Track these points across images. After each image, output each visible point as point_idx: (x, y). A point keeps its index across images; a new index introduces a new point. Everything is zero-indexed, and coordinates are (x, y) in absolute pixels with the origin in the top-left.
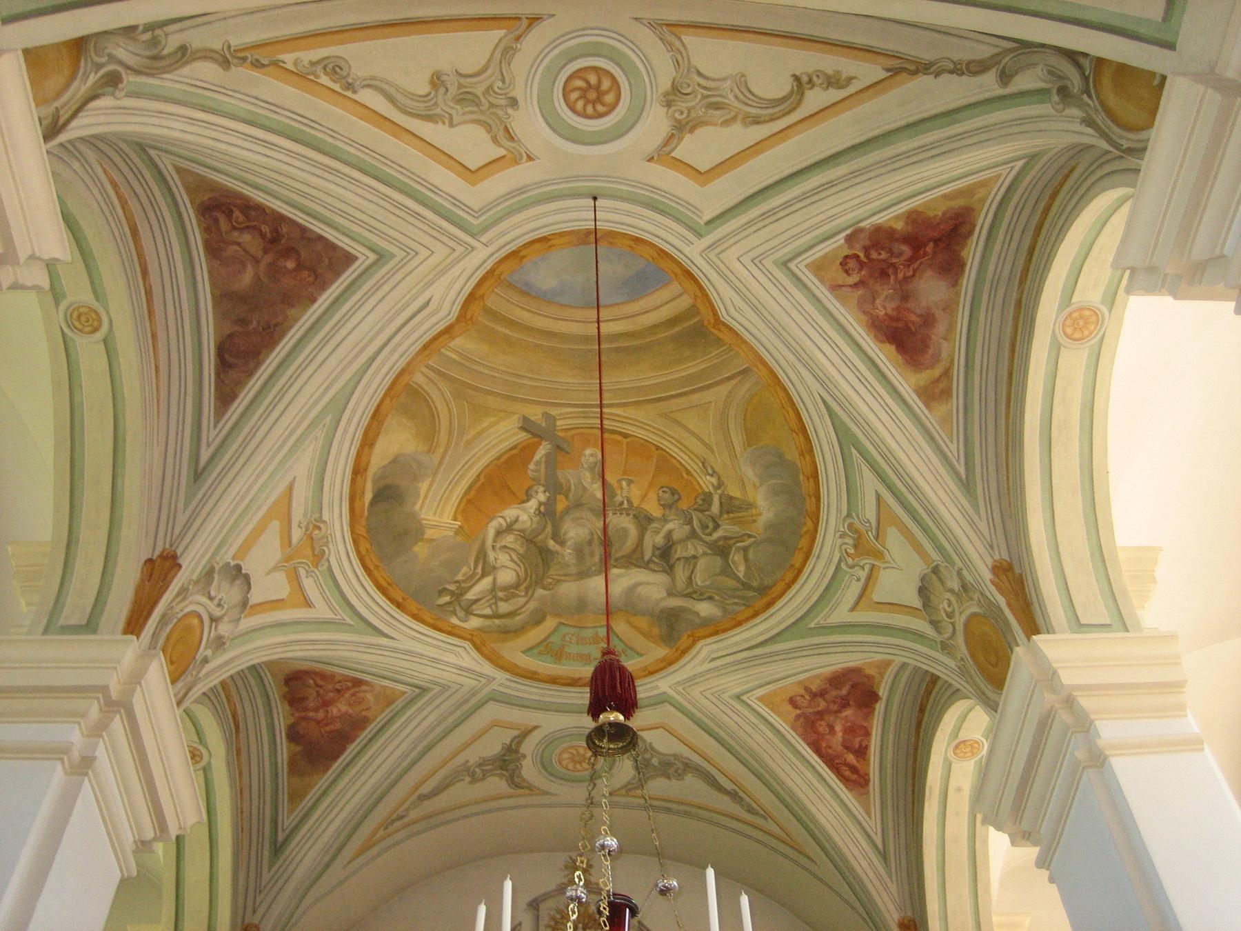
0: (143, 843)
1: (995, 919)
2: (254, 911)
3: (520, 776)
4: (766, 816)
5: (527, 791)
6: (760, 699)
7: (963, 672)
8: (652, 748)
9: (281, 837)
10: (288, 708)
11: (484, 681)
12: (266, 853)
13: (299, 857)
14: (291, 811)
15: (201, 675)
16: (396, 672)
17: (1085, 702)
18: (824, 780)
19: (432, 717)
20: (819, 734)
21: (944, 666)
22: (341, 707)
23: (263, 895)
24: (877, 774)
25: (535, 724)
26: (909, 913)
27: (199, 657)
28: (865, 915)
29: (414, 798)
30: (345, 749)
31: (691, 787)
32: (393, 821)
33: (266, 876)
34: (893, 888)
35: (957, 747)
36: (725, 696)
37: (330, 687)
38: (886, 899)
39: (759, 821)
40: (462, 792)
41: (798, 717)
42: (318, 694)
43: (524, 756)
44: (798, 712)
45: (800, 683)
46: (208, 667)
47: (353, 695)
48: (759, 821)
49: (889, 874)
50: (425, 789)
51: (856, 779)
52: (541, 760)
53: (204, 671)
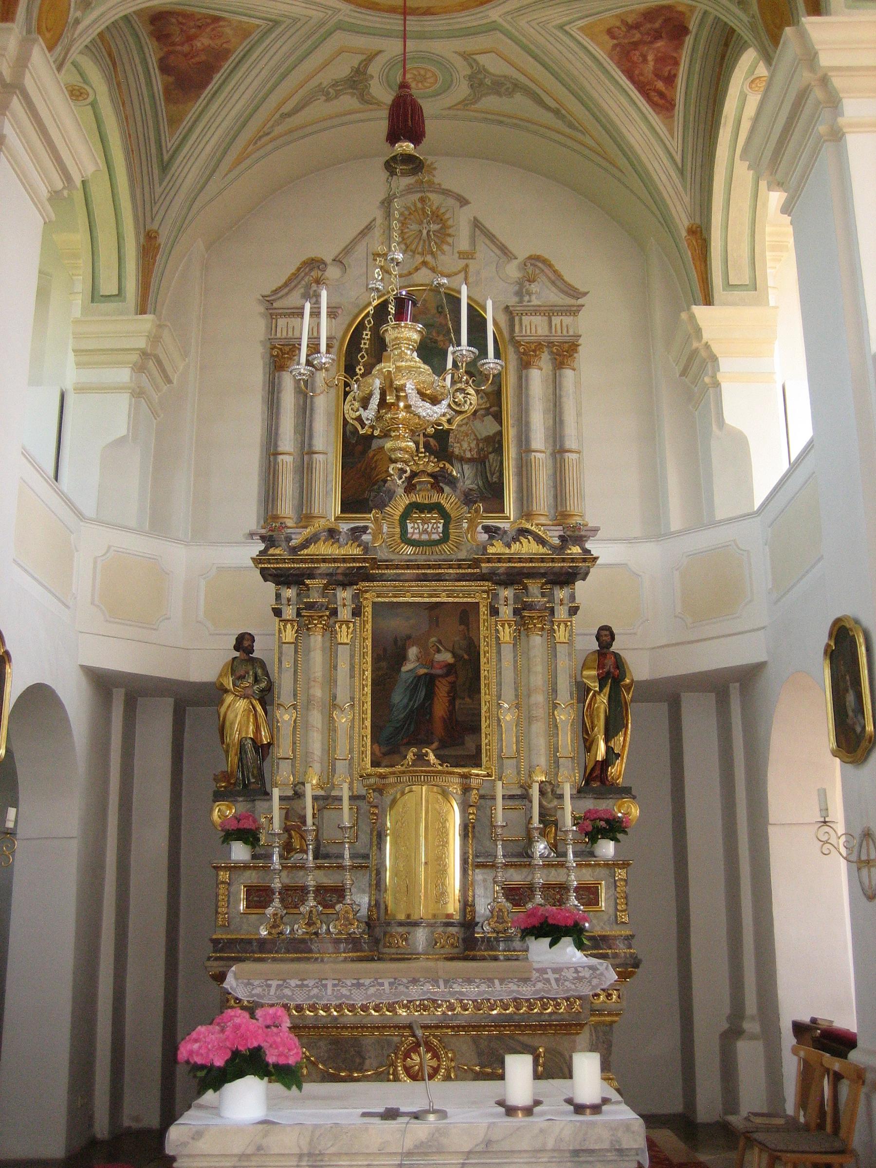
0: (55, 192)
1: (768, 229)
2: (153, 220)
3: (369, 93)
4: (584, 132)
5: (375, 107)
6: (581, 29)
7: (753, 28)
8: (485, 70)
9: (166, 158)
10: (156, 43)
11: (330, 12)
12: (156, 171)
13: (183, 175)
14: (172, 134)
15: (75, 36)
16: (249, 9)
17: (837, 82)
18: (635, 103)
19: (284, 49)
20: (633, 62)
21: (738, 20)
22: (203, 41)
23: (158, 204)
24: (682, 100)
25: (378, 49)
26: (698, 221)
27: (71, 20)
28: (661, 220)
29: (277, 116)
30: (212, 79)
31: (519, 104)
32: (260, 138)
33: (158, 190)
34: (687, 199)
35: (752, 82)
36: (550, 26)
37: (192, 24)
38: (679, 207)
39: (580, 136)
40: (319, 109)
41: (615, 46)
42: (182, 30)
43: (372, 77)
44: (615, 42)
45: (617, 16)
46: (81, 27)
47: (213, 30)
48: (580, 136)
49: (685, 188)
50: (286, 109)
51: (663, 104)
52: (388, 81)
53: (77, 32)
